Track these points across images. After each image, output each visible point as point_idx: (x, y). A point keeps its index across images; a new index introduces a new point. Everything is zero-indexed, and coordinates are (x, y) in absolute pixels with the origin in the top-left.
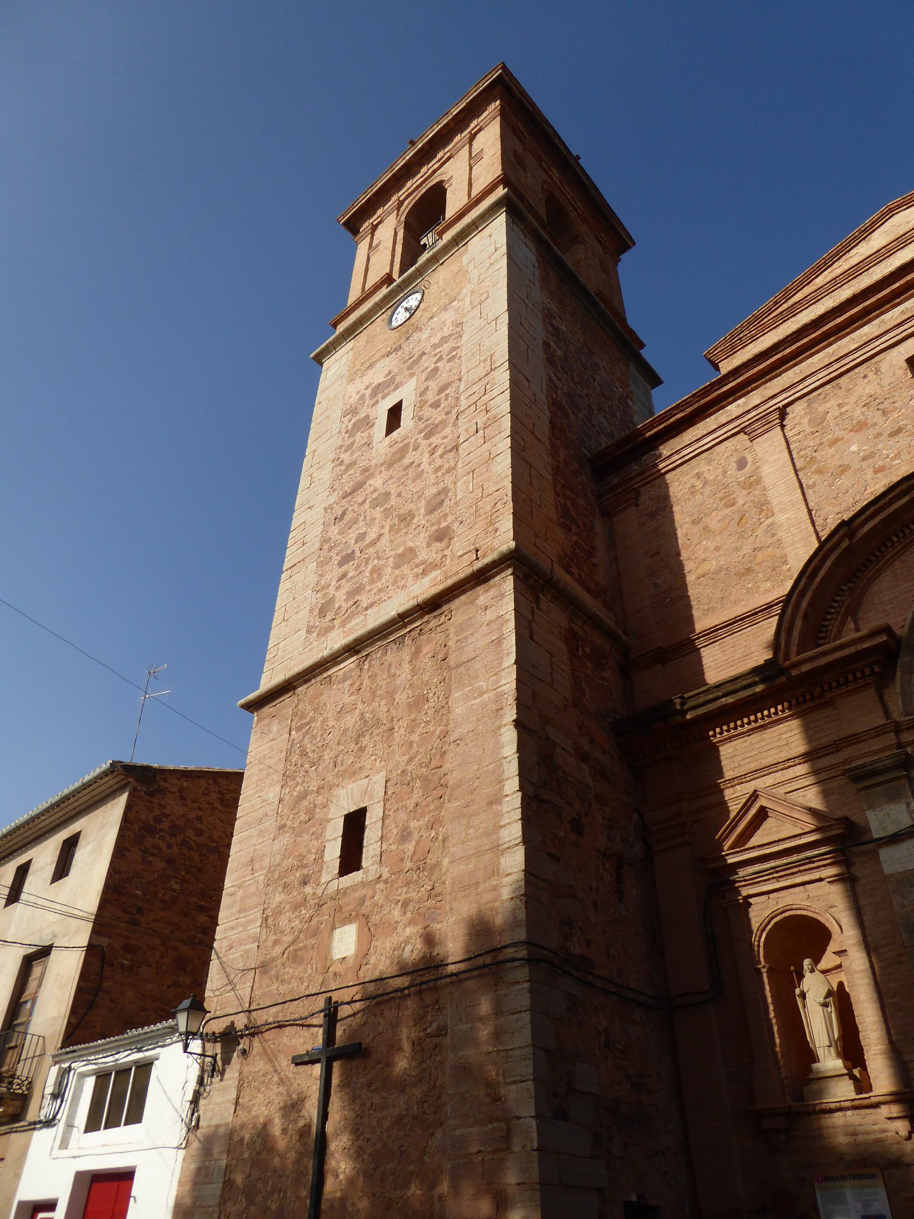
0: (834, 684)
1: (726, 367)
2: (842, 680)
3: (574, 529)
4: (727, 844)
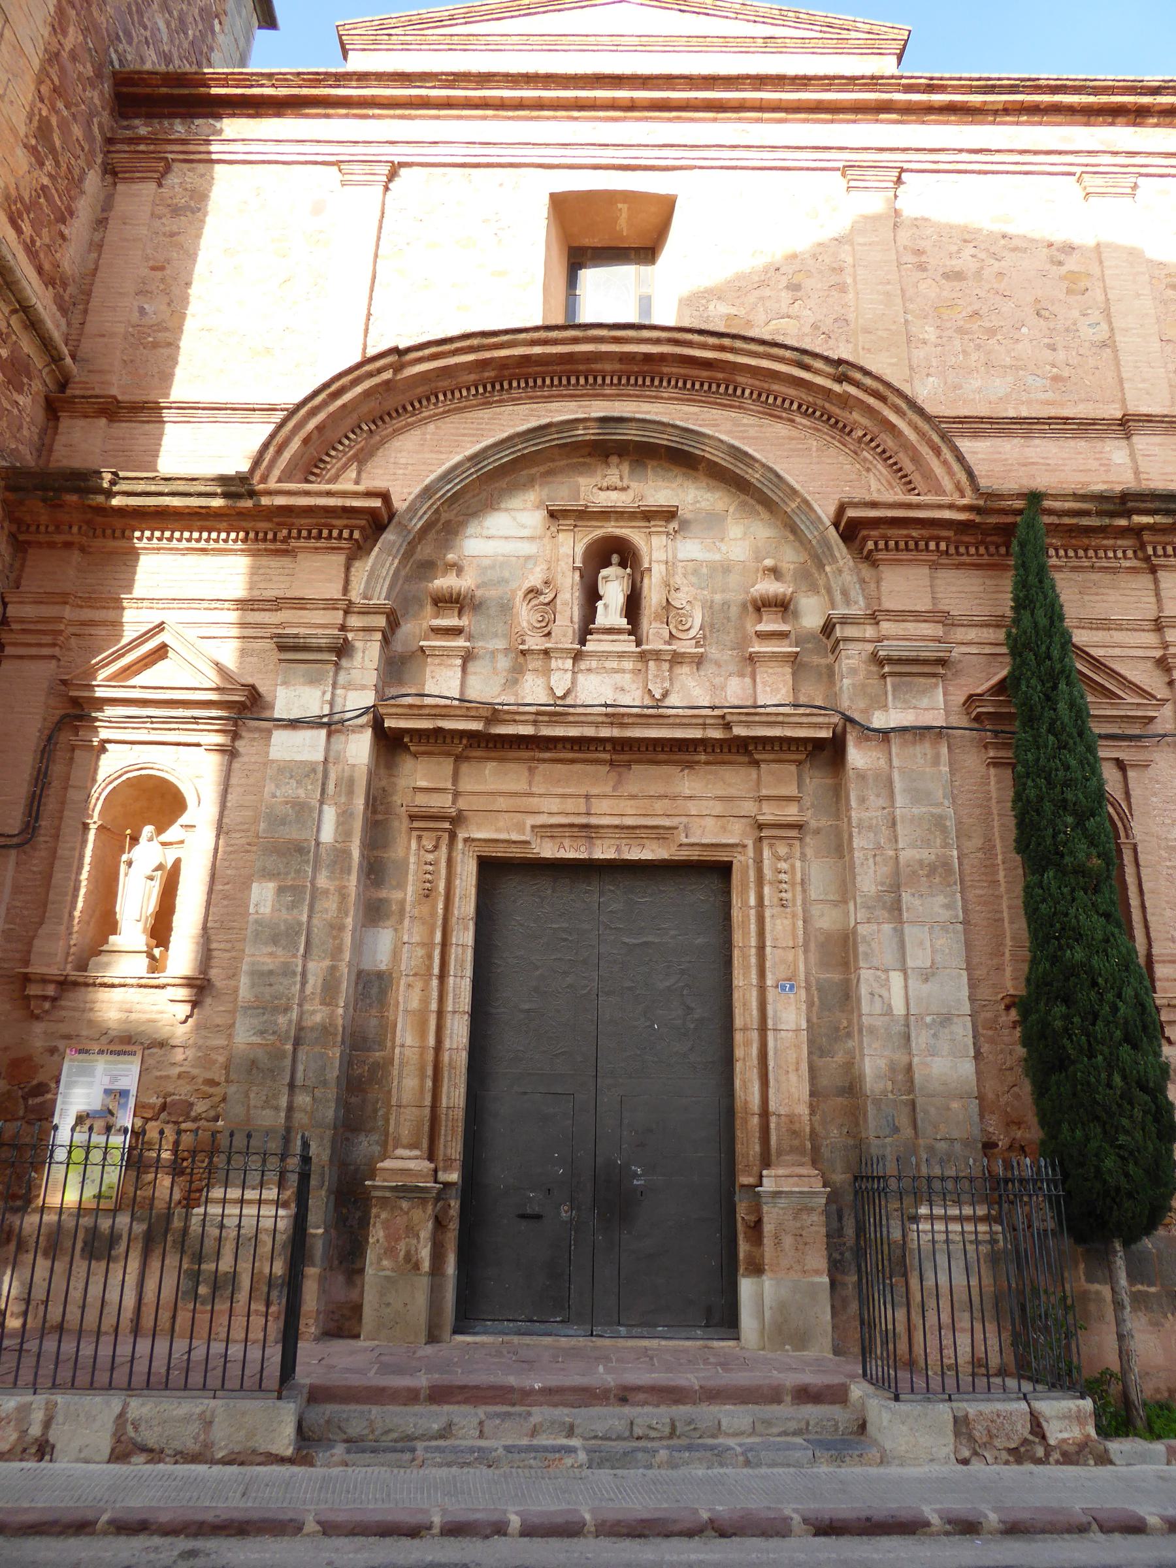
0: (304, 533)
1: (358, 62)
2: (314, 532)
3: (49, 165)
4: (102, 675)
